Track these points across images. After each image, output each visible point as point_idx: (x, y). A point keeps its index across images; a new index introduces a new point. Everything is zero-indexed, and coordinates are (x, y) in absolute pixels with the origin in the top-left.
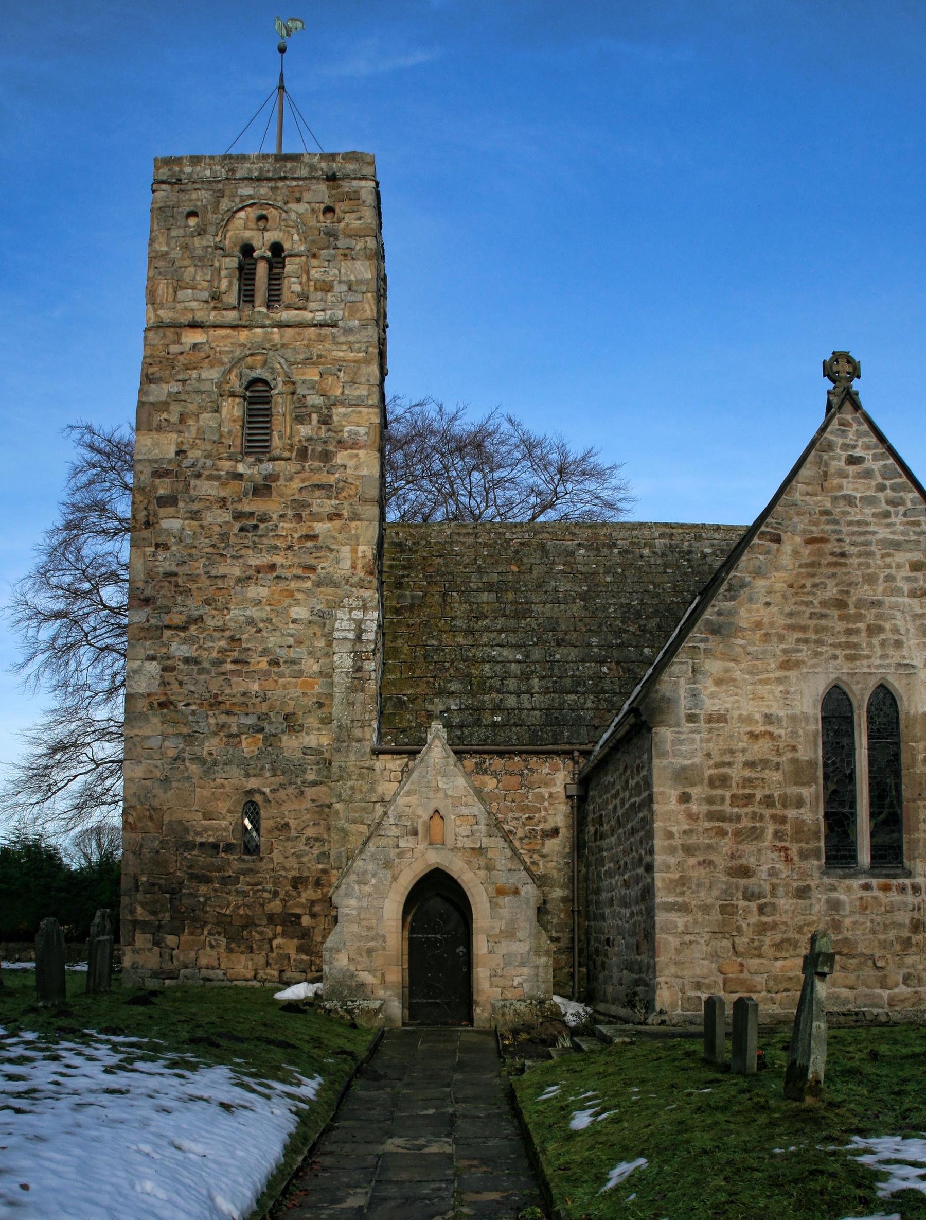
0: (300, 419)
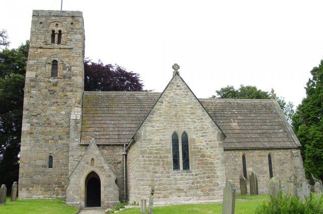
0: (64, 69)
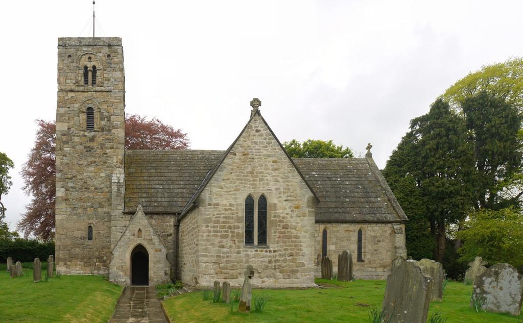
0: (102, 119)
